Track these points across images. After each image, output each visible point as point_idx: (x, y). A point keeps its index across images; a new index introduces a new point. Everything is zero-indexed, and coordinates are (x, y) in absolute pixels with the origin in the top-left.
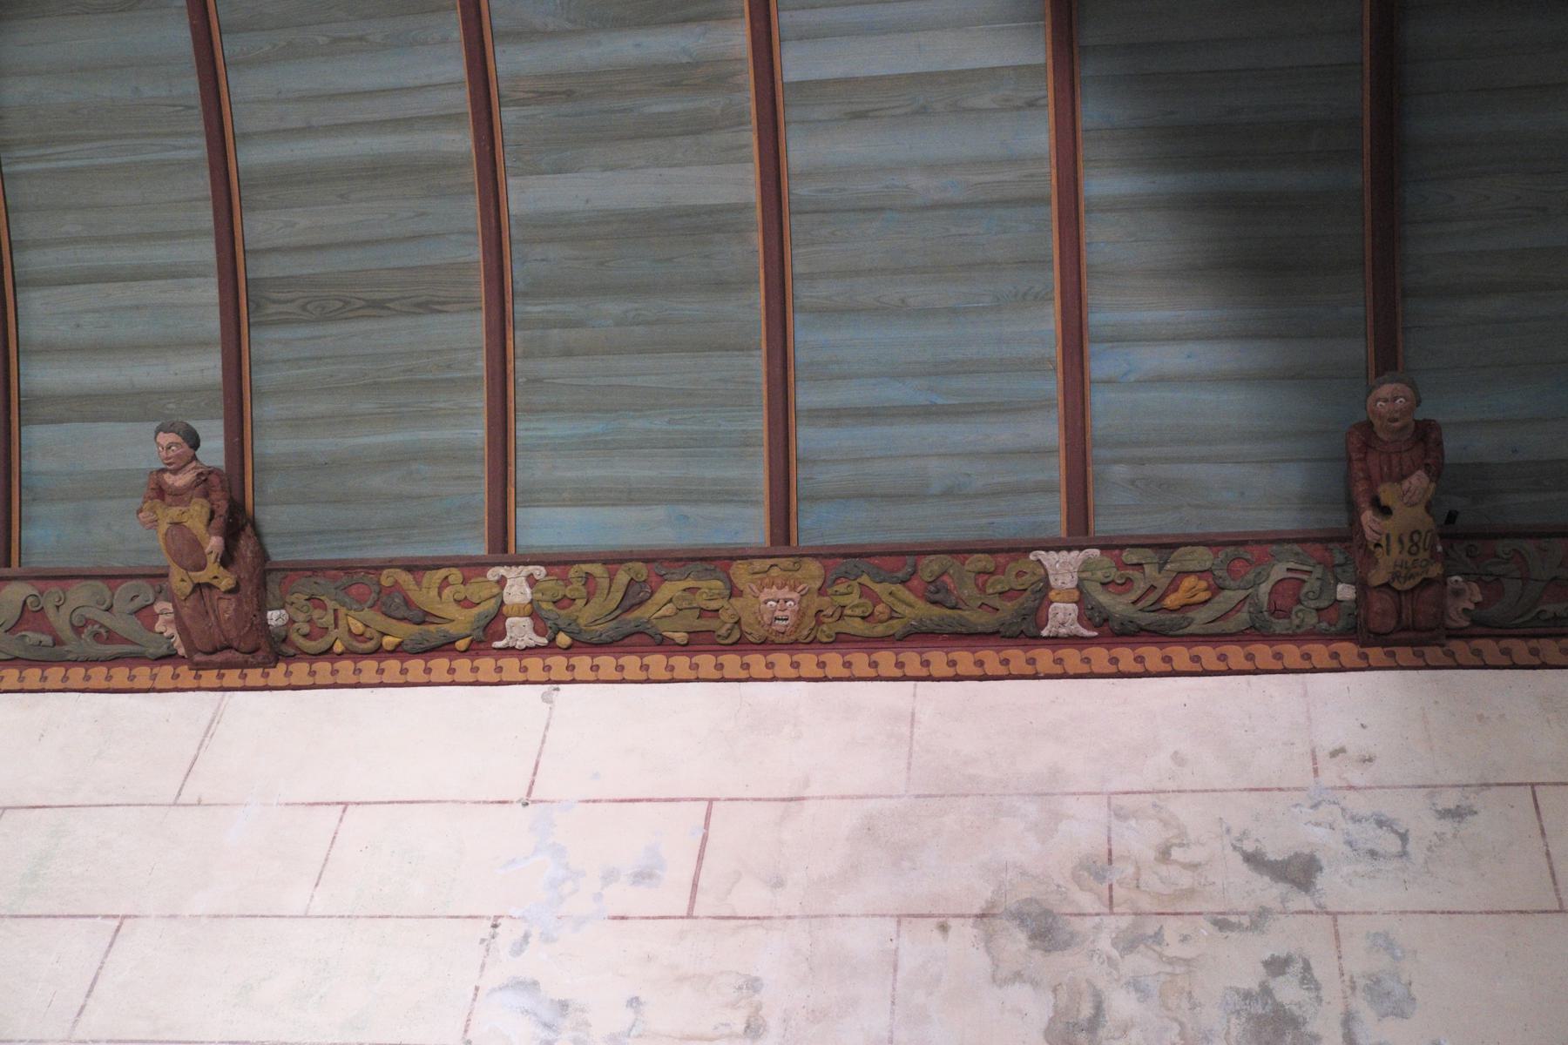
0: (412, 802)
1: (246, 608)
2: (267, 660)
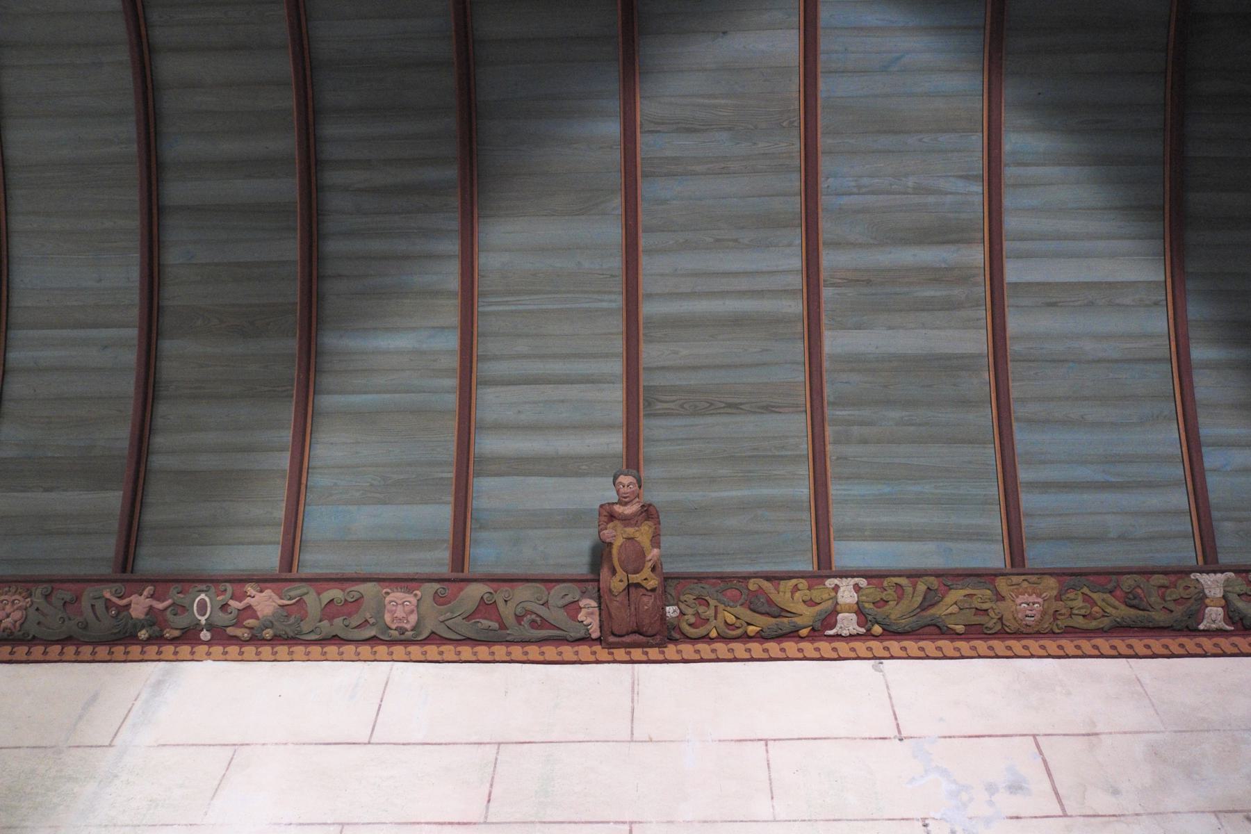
0: (815, 739)
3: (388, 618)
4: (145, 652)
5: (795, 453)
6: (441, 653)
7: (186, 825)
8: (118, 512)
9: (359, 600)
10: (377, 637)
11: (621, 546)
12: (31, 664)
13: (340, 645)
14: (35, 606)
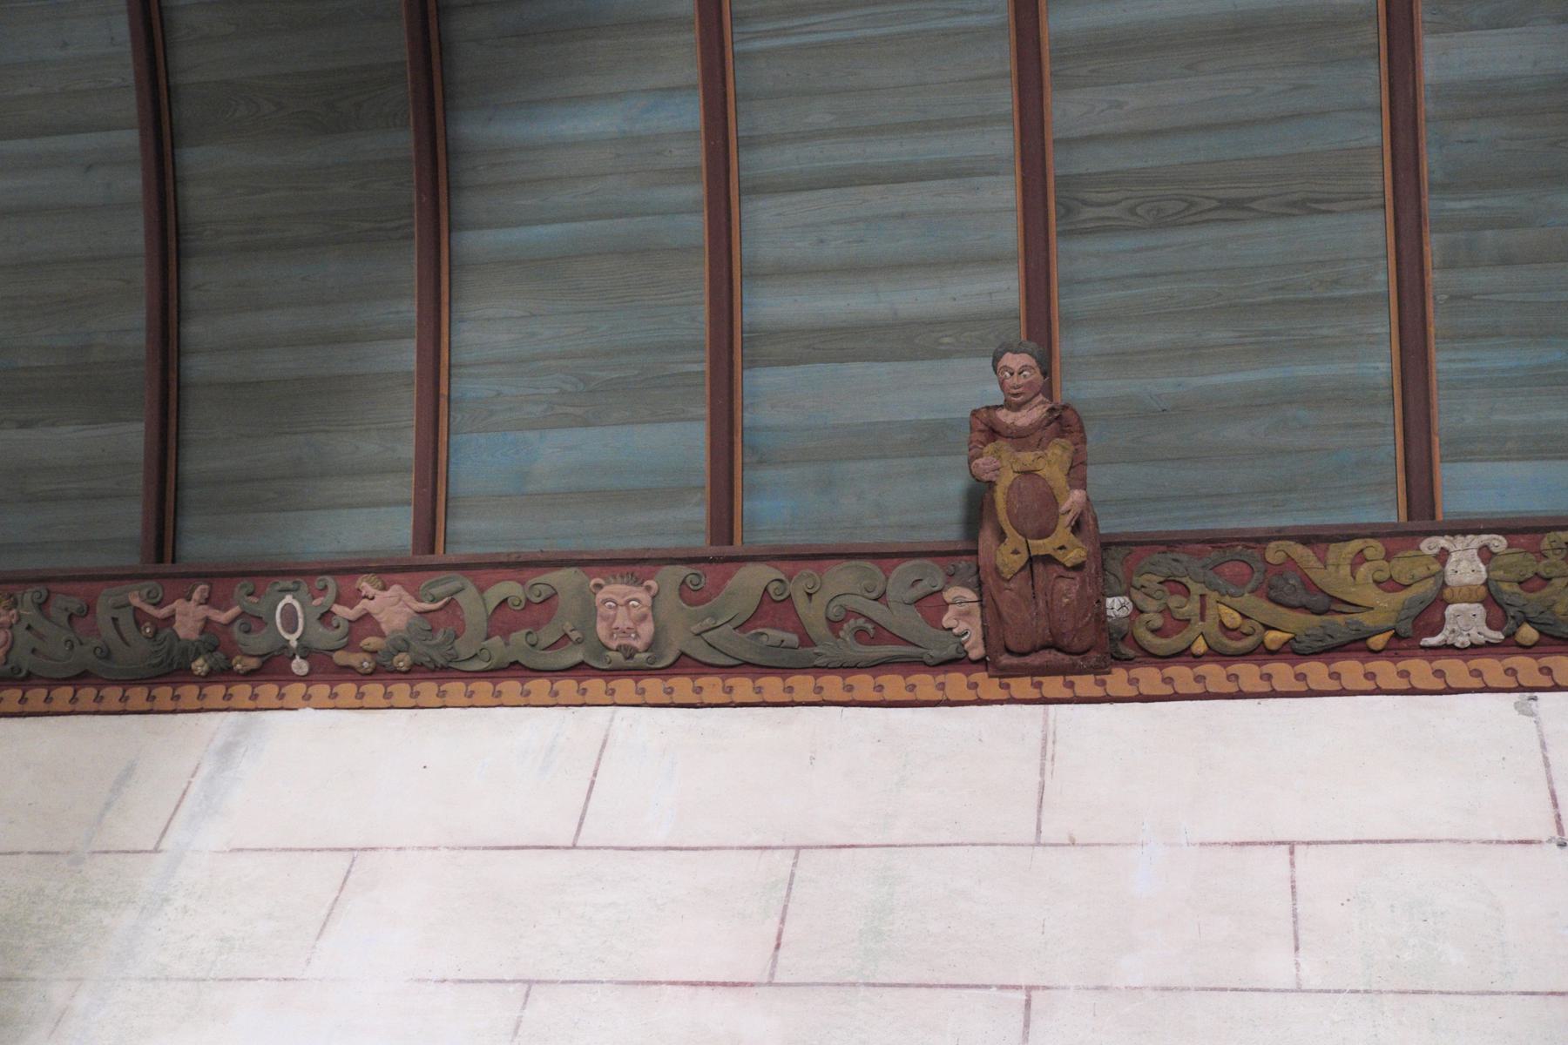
0: (1389, 842)
1: (1090, 591)
2: (1103, 664)
3: (602, 630)
4: (205, 696)
5: (1364, 291)
6: (699, 690)
7: (278, 980)
8: (141, 458)
9: (549, 600)
10: (588, 665)
11: (1011, 487)
12: (28, 719)
13: (523, 679)
14: (24, 624)
